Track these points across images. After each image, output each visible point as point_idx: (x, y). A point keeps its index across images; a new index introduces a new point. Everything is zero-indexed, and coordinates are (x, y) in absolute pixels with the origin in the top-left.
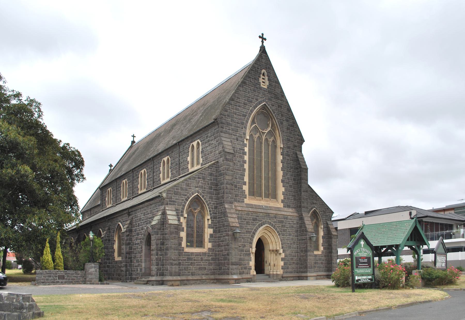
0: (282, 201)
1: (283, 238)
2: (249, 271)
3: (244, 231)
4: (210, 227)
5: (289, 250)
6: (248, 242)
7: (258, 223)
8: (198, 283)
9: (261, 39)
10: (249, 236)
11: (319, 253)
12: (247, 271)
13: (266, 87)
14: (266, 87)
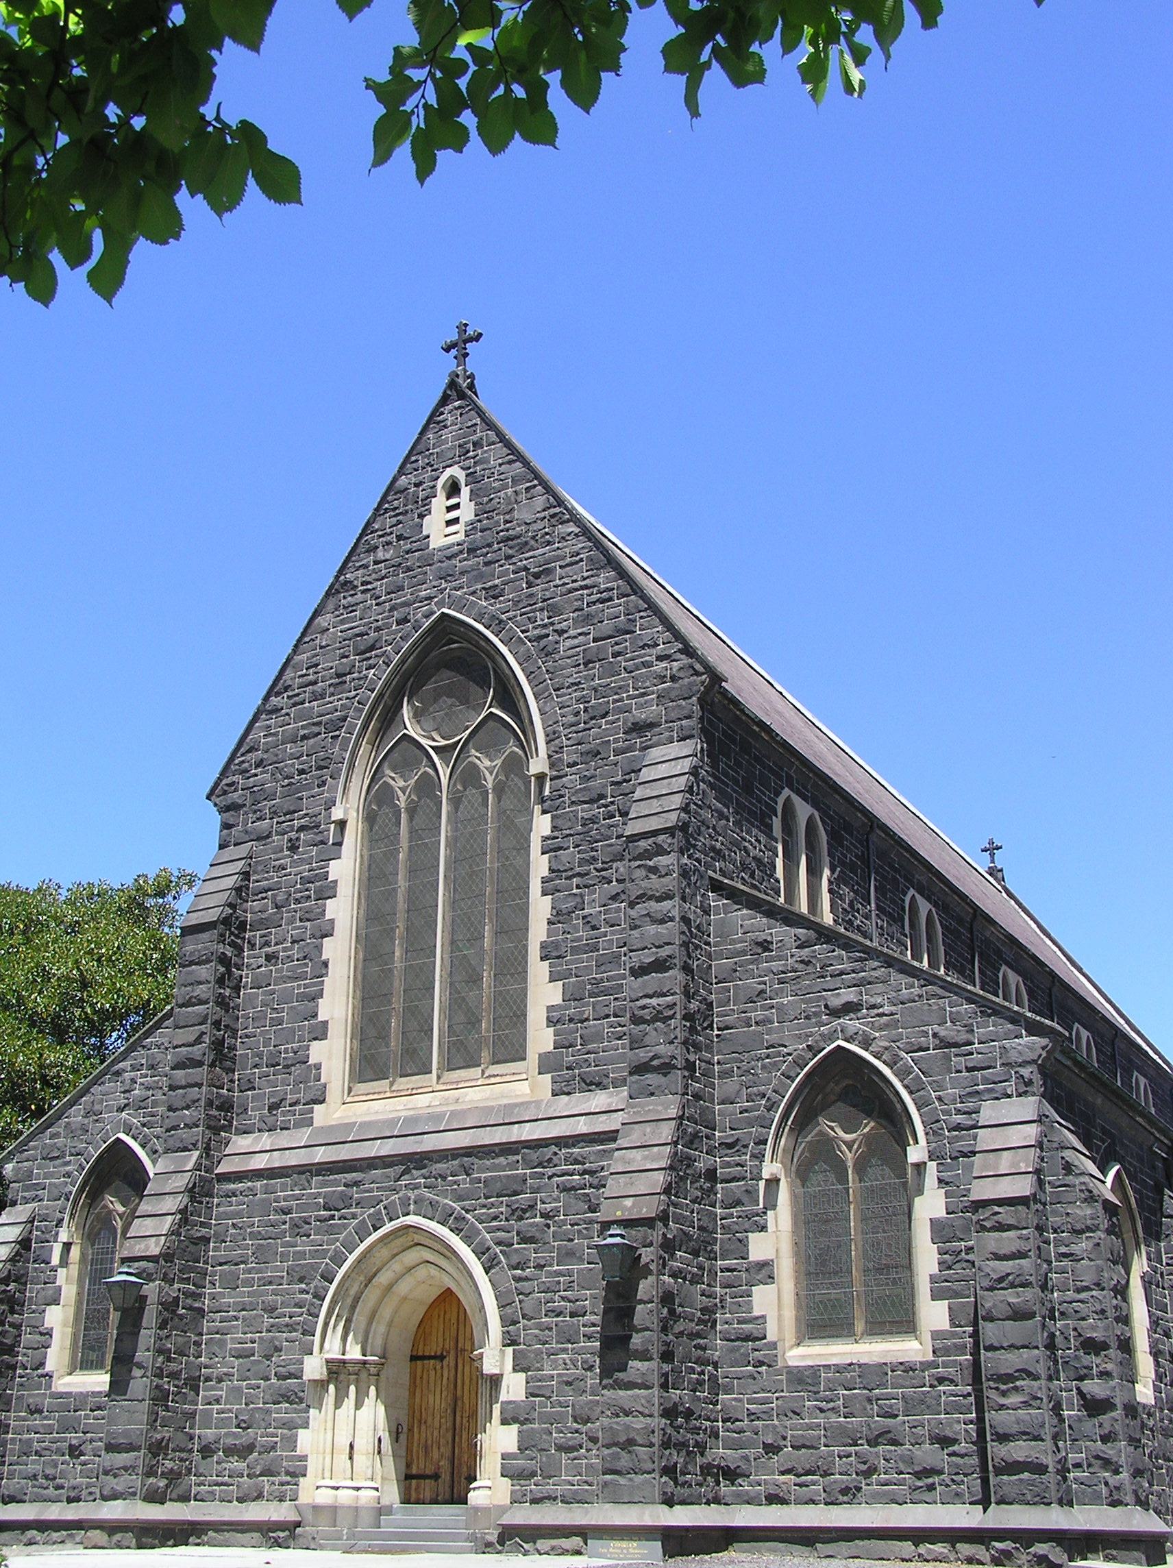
0: (546, 1064)
1: (518, 1279)
2: (288, 1483)
3: (276, 1269)
4: (765, 1273)
5: (565, 1350)
6: (291, 1328)
7: (354, 1216)
8: (78, 1539)
9: (455, 337)
10: (302, 1292)
11: (912, 1349)
12: (282, 1484)
13: (437, 542)
14: (437, 542)
